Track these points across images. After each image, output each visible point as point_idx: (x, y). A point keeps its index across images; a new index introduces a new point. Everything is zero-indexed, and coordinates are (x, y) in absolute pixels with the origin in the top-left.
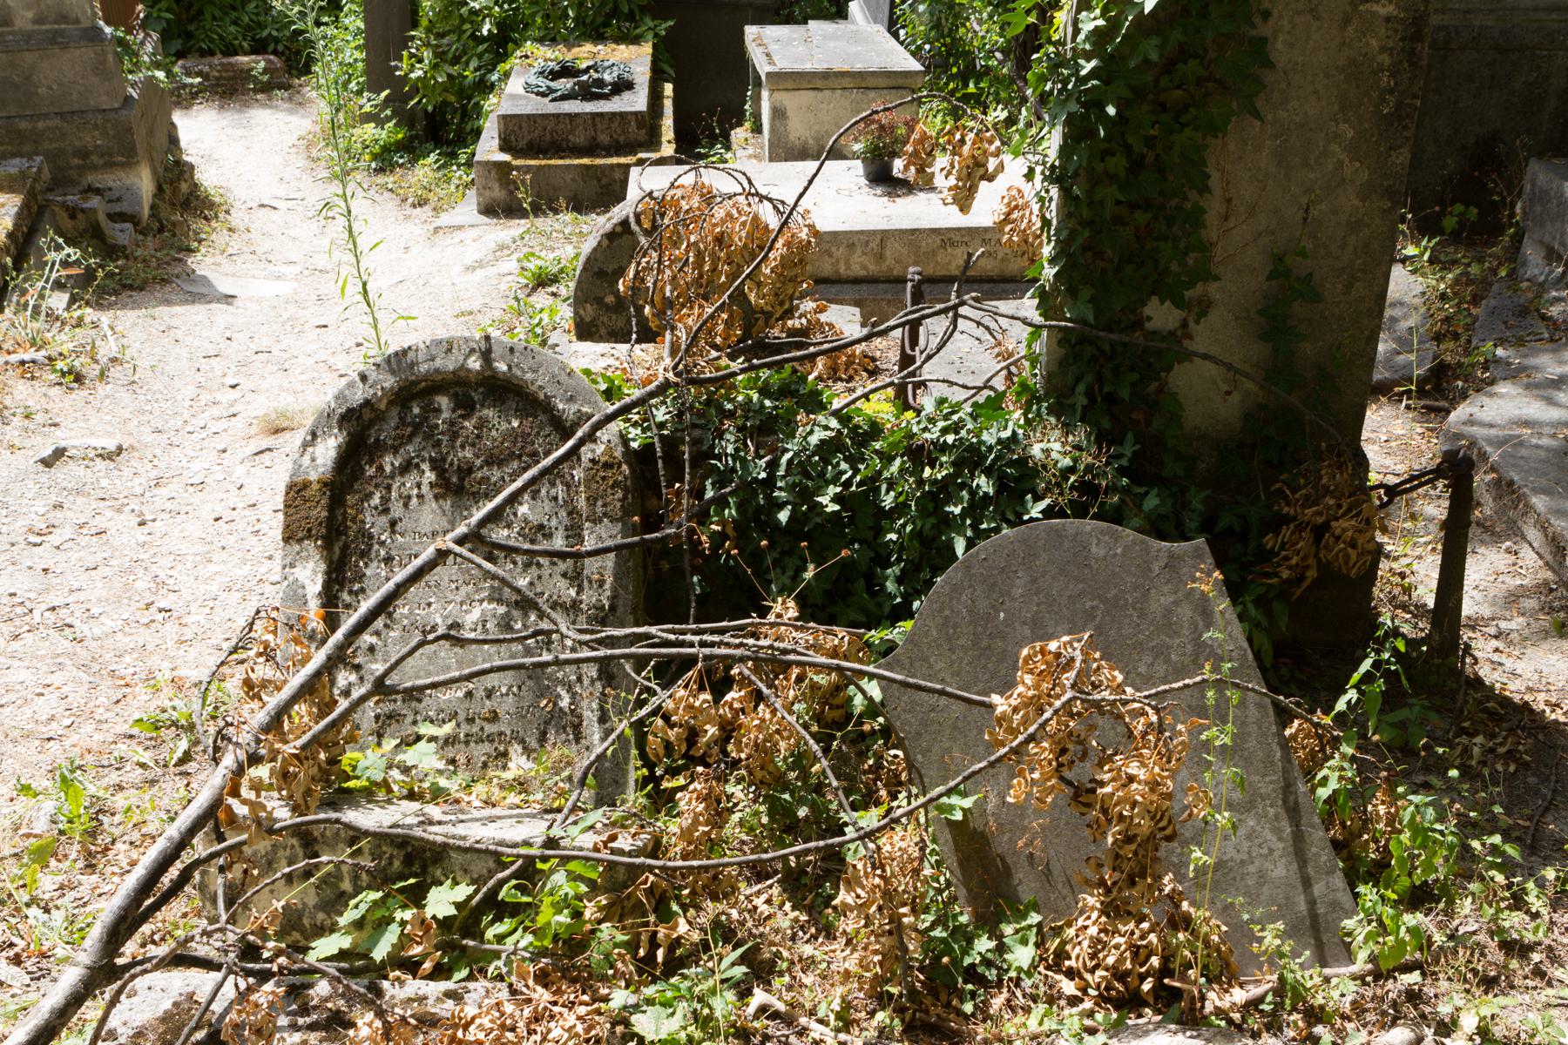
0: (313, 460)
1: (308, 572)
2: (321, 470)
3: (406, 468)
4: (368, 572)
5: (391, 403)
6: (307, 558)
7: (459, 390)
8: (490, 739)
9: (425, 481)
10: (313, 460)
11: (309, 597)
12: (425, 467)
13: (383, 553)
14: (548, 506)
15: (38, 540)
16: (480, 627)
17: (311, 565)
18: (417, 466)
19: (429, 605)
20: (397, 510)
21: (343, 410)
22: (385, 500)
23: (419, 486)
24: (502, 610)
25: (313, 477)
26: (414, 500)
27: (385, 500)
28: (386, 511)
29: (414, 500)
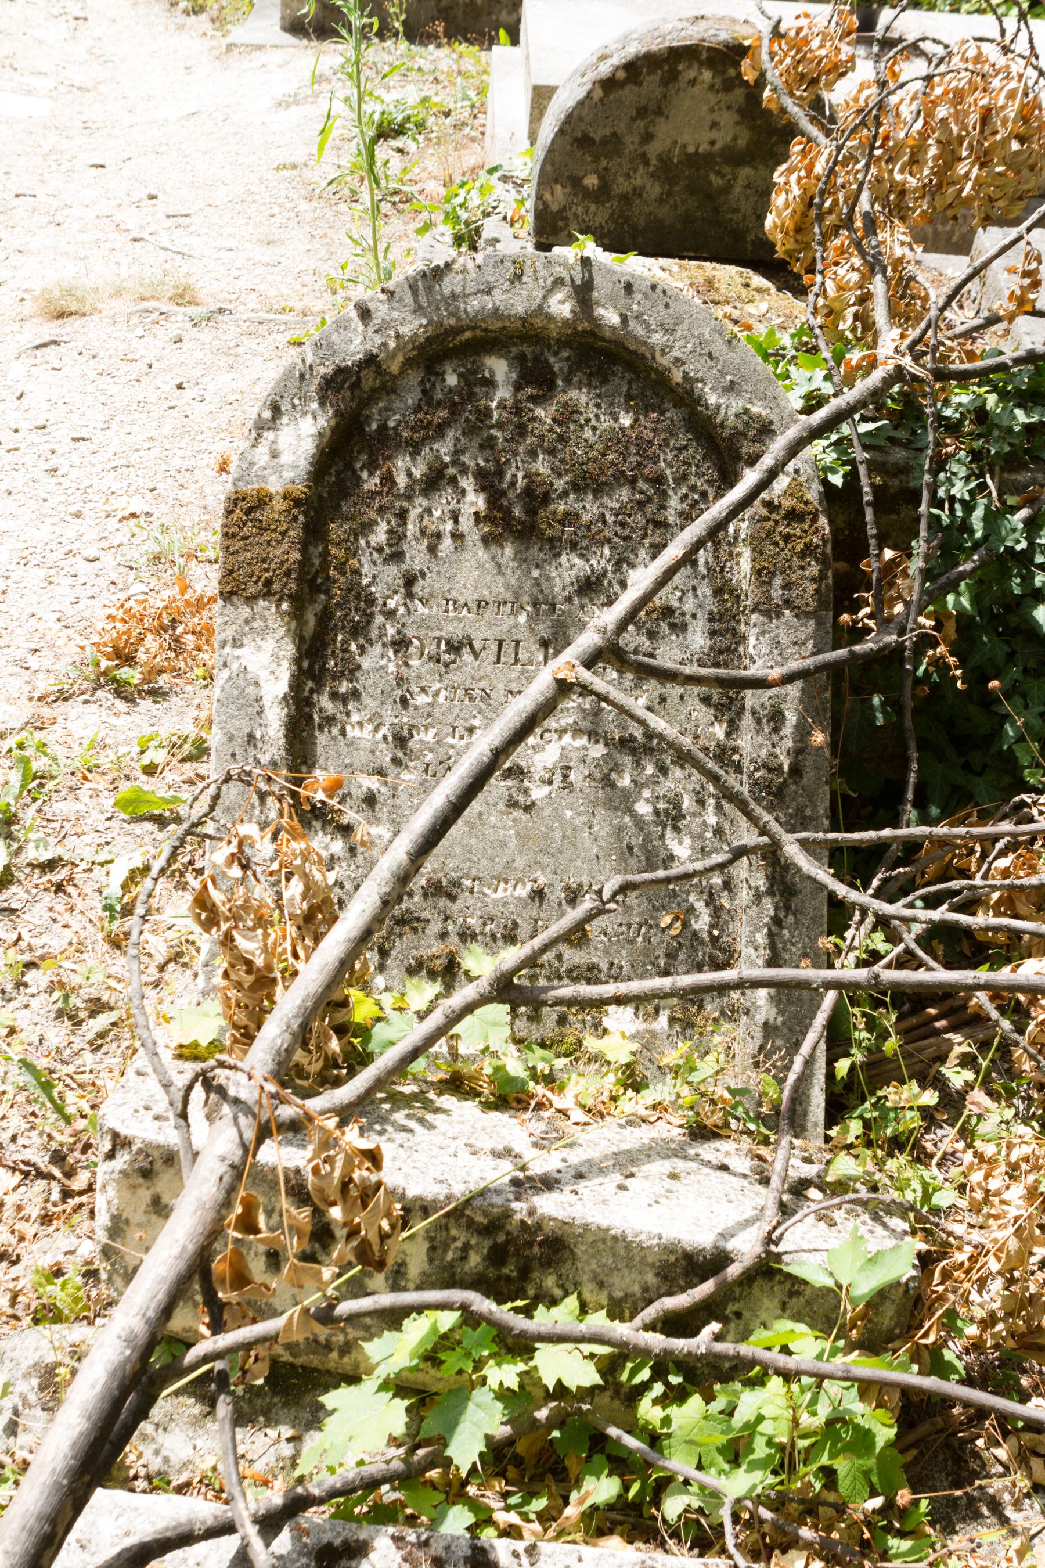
0: (275, 455)
1: (265, 658)
2: (289, 475)
3: (435, 480)
4: (365, 663)
5: (409, 363)
7: (528, 350)
10: (275, 455)
11: (266, 702)
12: (467, 483)
13: (391, 631)
16: (558, 778)
18: (453, 481)
20: (416, 556)
21: (327, 370)
22: (396, 537)
23: (455, 517)
27: (396, 537)
28: (397, 556)
29: (447, 543)
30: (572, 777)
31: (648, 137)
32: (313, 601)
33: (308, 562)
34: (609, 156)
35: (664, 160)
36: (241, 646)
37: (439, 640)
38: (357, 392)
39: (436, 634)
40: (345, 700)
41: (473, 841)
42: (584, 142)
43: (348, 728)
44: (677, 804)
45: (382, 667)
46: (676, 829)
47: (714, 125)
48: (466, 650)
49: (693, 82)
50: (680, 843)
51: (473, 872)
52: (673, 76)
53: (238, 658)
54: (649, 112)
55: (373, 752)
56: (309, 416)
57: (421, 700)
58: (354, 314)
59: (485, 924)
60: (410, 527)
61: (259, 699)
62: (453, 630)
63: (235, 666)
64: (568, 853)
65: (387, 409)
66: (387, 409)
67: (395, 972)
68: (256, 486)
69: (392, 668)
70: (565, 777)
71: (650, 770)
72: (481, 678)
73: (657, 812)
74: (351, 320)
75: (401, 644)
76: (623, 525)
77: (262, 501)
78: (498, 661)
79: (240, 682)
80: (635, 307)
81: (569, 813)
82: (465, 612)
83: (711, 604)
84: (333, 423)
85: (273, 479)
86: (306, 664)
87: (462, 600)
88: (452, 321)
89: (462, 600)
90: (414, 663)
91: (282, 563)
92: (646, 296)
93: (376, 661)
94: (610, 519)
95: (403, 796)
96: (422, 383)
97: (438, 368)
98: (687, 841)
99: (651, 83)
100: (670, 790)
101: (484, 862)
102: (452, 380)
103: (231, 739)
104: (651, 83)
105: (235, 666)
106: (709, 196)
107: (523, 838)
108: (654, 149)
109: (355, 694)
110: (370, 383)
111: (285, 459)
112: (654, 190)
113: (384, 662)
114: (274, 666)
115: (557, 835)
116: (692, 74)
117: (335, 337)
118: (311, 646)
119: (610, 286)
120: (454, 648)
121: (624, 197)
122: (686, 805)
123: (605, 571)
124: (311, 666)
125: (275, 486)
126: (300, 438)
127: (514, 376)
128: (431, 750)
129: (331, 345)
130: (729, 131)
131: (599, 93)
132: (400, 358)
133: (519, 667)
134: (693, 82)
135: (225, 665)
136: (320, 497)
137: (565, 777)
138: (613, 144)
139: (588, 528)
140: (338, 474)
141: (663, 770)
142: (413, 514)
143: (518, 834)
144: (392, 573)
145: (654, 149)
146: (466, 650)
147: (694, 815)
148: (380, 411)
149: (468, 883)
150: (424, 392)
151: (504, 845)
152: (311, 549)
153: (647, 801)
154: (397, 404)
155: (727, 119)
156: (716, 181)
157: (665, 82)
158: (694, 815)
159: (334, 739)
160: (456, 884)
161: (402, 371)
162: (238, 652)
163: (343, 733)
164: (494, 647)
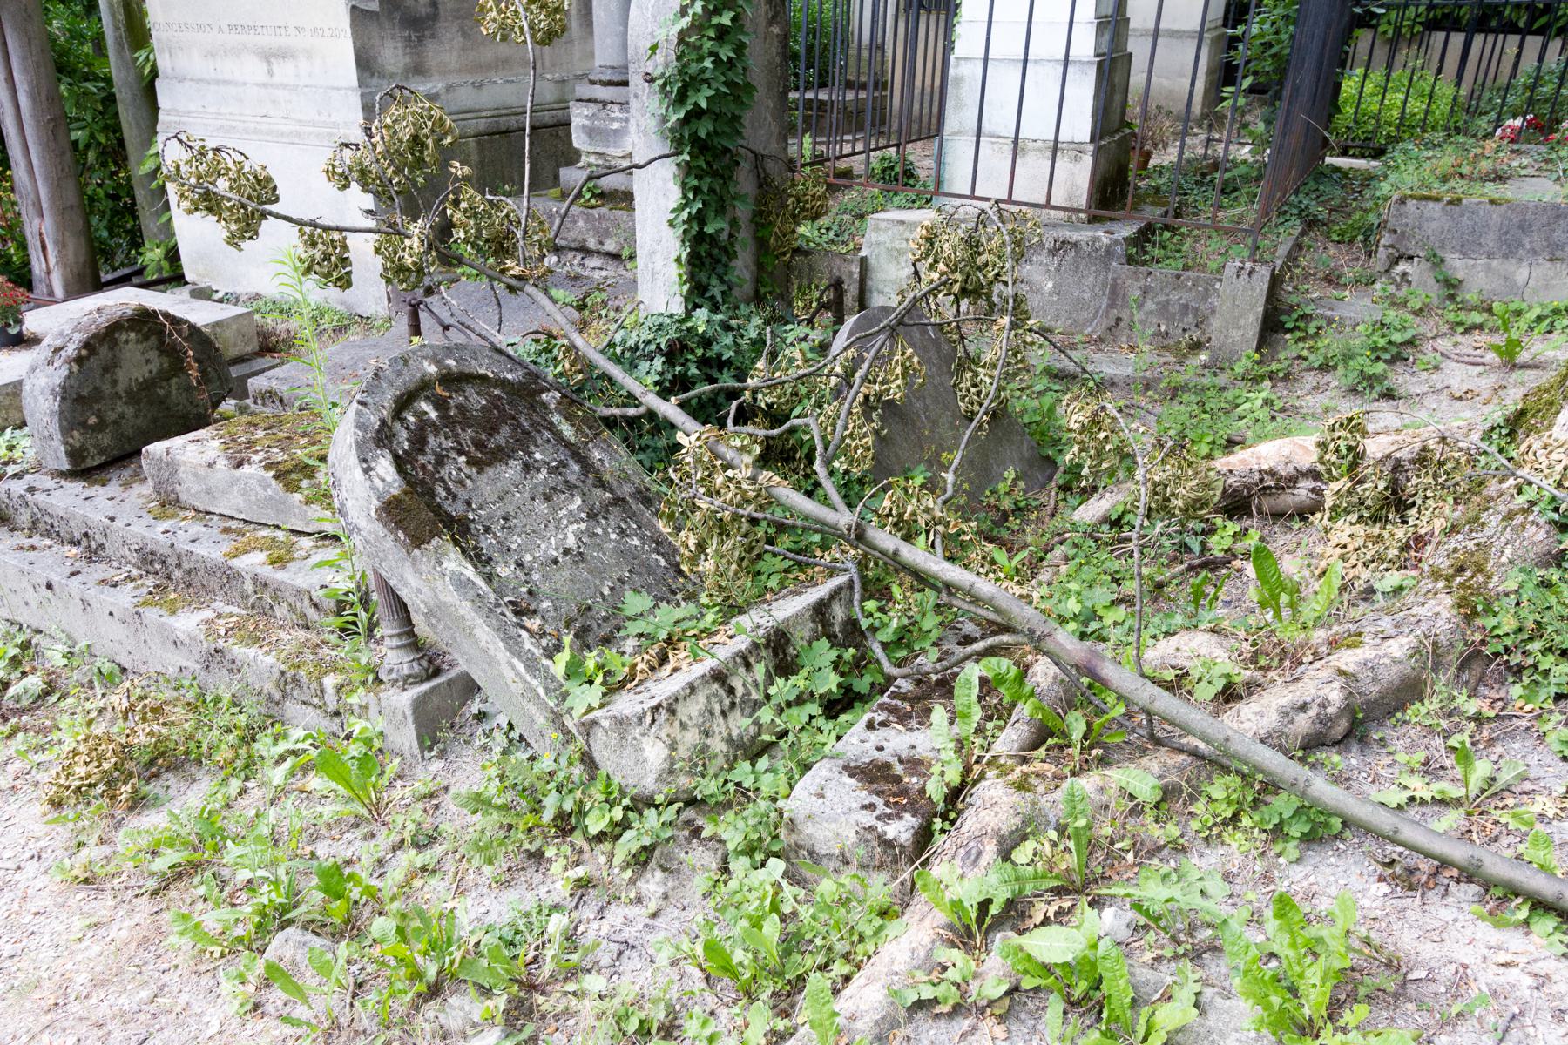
0: (383, 480)
3: (441, 460)
9: (463, 466)
10: (383, 480)
12: (453, 454)
20: (463, 494)
22: (447, 489)
24: (583, 526)
27: (447, 489)
28: (455, 497)
31: (115, 382)
34: (97, 402)
35: (129, 392)
42: (79, 400)
47: (148, 361)
49: (127, 342)
52: (114, 344)
54: (109, 368)
57: (514, 547)
75: (487, 530)
99: (104, 351)
102: (412, 419)
104: (104, 351)
106: (162, 403)
108: (121, 388)
111: (389, 479)
112: (130, 411)
116: (124, 337)
121: (115, 422)
125: (395, 492)
130: (157, 363)
131: (75, 368)
134: (127, 342)
138: (97, 395)
145: (121, 388)
155: (153, 355)
156: (161, 392)
157: (111, 349)
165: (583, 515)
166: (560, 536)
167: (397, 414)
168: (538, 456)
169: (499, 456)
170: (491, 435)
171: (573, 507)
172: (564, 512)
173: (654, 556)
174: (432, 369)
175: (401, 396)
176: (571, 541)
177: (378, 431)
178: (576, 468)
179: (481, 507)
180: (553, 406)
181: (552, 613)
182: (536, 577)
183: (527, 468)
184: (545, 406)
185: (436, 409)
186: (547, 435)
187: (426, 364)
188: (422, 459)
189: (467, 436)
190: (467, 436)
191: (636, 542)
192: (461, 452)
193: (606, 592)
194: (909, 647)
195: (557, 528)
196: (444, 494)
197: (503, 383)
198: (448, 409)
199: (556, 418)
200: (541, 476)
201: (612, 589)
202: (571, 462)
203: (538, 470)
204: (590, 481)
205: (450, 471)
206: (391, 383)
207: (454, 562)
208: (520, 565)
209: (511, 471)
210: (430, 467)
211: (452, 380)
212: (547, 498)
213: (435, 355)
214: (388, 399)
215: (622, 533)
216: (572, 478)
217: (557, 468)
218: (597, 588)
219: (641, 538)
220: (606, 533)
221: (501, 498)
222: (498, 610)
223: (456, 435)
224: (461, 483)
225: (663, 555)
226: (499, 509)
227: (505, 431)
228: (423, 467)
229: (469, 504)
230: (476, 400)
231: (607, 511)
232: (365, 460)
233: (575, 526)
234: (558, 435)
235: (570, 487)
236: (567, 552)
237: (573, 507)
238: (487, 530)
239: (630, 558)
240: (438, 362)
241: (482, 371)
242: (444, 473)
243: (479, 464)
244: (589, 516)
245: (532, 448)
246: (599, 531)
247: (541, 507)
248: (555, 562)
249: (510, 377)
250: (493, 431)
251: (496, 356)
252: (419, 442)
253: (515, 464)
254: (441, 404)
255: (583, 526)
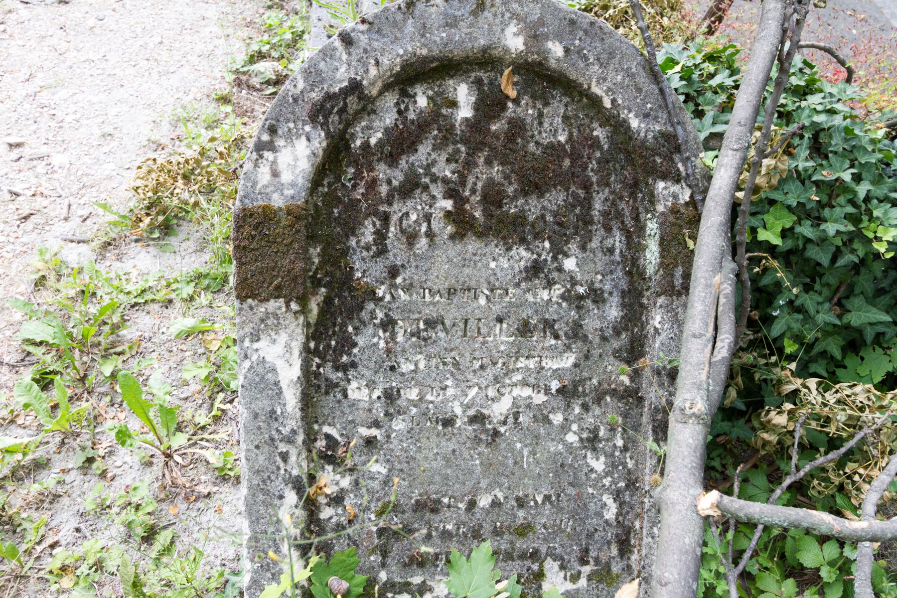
0: (275, 174)
1: (279, 348)
2: (289, 192)
3: (410, 187)
4: (361, 341)
5: (387, 87)
6: (277, 328)
7: (483, 75)
8: (523, 556)
9: (437, 215)
10: (275, 174)
11: (284, 384)
12: (437, 190)
13: (380, 315)
14: (601, 261)
15: (181, 130)
16: (511, 420)
17: (283, 337)
18: (426, 188)
19: (444, 389)
20: (397, 252)
21: (316, 95)
22: (381, 236)
23: (428, 218)
24: (539, 398)
25: (278, 201)
26: (423, 241)
27: (381, 236)
28: (382, 251)
29: (423, 241)
30: (521, 419)
32: (315, 293)
33: (308, 260)
36: (259, 340)
37: (418, 320)
38: (344, 116)
39: (417, 316)
40: (345, 368)
41: (449, 471)
43: (350, 392)
44: (595, 431)
45: (374, 345)
46: (594, 449)
48: (440, 327)
50: (597, 459)
51: (450, 493)
53: (257, 350)
55: (370, 410)
56: (304, 138)
58: (338, 43)
59: (458, 528)
60: (392, 229)
61: (277, 384)
62: (429, 312)
63: (254, 358)
64: (518, 474)
65: (369, 128)
66: (369, 128)
67: (394, 568)
68: (261, 203)
69: (382, 344)
70: (516, 419)
71: (577, 410)
72: (452, 350)
73: (581, 439)
74: (335, 49)
76: (560, 224)
77: (267, 215)
78: (465, 335)
79: (261, 370)
80: (577, 42)
81: (519, 445)
82: (437, 298)
83: (624, 284)
84: (324, 144)
85: (275, 196)
86: (312, 345)
87: (435, 288)
88: (425, 52)
89: (435, 288)
90: (400, 338)
91: (289, 272)
92: (586, 32)
93: (369, 340)
94: (549, 218)
95: (395, 442)
96: (397, 104)
97: (411, 91)
98: (602, 459)
100: (591, 424)
101: (457, 486)
102: (422, 102)
103: (256, 416)
105: (254, 358)
107: (487, 466)
109: (354, 365)
110: (354, 106)
113: (375, 340)
114: (288, 355)
115: (511, 462)
117: (322, 65)
118: (316, 331)
119: (557, 23)
120: (431, 324)
122: (601, 434)
123: (546, 260)
124: (317, 347)
126: (296, 160)
127: (473, 99)
128: (415, 406)
129: (319, 73)
132: (379, 84)
133: (481, 339)
135: (246, 357)
136: (316, 205)
137: (516, 419)
139: (533, 226)
140: (329, 185)
141: (585, 407)
142: (394, 219)
143: (482, 463)
144: (378, 269)
146: (440, 327)
147: (608, 440)
148: (363, 129)
149: (446, 500)
150: (400, 112)
151: (471, 472)
152: (311, 250)
153: (575, 433)
154: (377, 124)
158: (608, 440)
159: (339, 402)
160: (439, 501)
161: (381, 93)
162: (256, 345)
163: (346, 396)
164: (462, 325)
165: (555, 385)
166: (491, 393)
167: (405, 79)
168: (570, 264)
169: (508, 229)
170: (525, 193)
171: (551, 364)
172: (532, 364)
173: (608, 499)
174: (514, 42)
175: (425, 60)
176: (500, 409)
177: (329, 97)
178: (614, 312)
179: (408, 288)
180: (660, 208)
181: (376, 485)
182: (399, 425)
183: (535, 270)
184: (652, 199)
185: (477, 107)
186: (617, 240)
187: (512, 29)
188: (382, 171)
189: (487, 172)
190: (487, 172)
191: (599, 465)
192: (451, 194)
193: (484, 501)
194: (836, 304)
195: (496, 380)
196: (370, 238)
197: (619, 127)
198: (495, 117)
199: (652, 226)
200: (545, 295)
201: (495, 504)
202: (615, 300)
203: (549, 284)
204: (616, 344)
205: (410, 211)
206: (424, 30)
207: (282, 353)
208: (390, 396)
209: (505, 262)
210: (384, 189)
211: (539, 77)
212: (525, 329)
213: (541, 22)
214: (393, 55)
215: (592, 441)
216: (591, 324)
217: (581, 298)
218: (476, 490)
219: (613, 465)
220: (565, 428)
221: (451, 292)
222: (283, 447)
223: (469, 164)
224: (411, 238)
225: (621, 505)
226: (433, 305)
227: (556, 198)
228: (373, 184)
229: (393, 272)
230: (553, 126)
231: (599, 400)
232: (273, 130)
233: (527, 392)
234: (634, 246)
235: (576, 333)
236: (478, 419)
237: (551, 364)
238: (388, 324)
239: (565, 480)
240: (534, 36)
241: (596, 90)
242: (397, 209)
243: (462, 224)
244: (561, 391)
245: (573, 247)
246: (557, 418)
247: (502, 338)
248: (448, 422)
249: (634, 123)
250: (533, 186)
251: (643, 79)
252: (401, 142)
253: (523, 256)
254: (490, 104)
255: (539, 398)
